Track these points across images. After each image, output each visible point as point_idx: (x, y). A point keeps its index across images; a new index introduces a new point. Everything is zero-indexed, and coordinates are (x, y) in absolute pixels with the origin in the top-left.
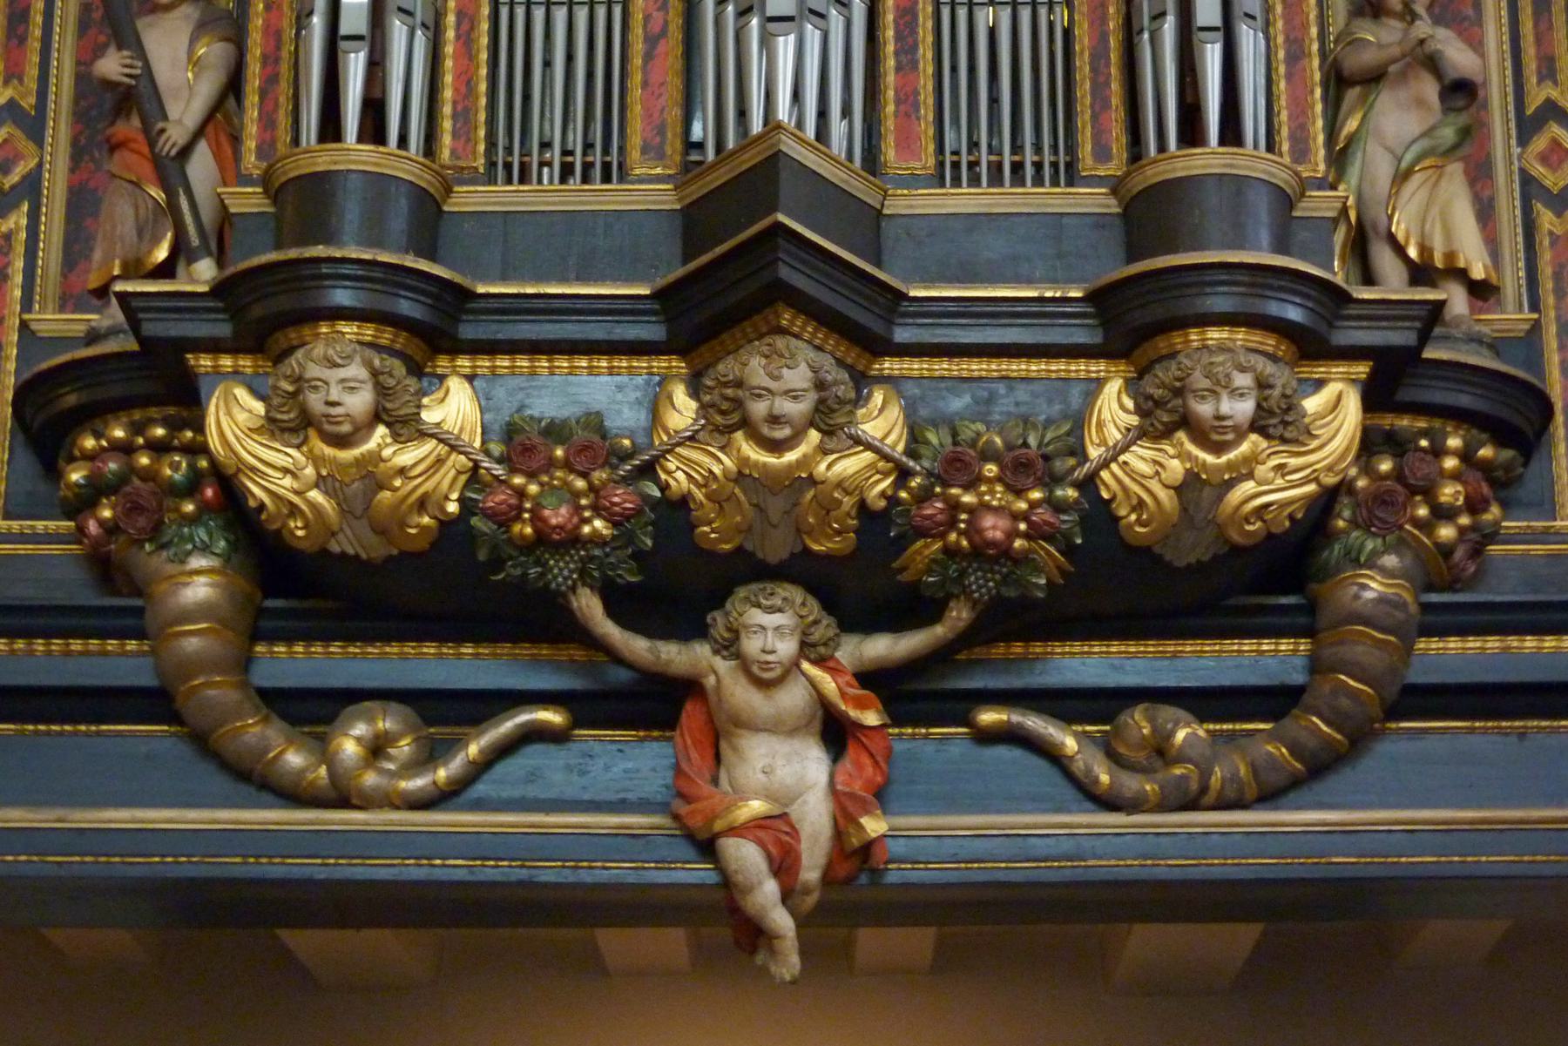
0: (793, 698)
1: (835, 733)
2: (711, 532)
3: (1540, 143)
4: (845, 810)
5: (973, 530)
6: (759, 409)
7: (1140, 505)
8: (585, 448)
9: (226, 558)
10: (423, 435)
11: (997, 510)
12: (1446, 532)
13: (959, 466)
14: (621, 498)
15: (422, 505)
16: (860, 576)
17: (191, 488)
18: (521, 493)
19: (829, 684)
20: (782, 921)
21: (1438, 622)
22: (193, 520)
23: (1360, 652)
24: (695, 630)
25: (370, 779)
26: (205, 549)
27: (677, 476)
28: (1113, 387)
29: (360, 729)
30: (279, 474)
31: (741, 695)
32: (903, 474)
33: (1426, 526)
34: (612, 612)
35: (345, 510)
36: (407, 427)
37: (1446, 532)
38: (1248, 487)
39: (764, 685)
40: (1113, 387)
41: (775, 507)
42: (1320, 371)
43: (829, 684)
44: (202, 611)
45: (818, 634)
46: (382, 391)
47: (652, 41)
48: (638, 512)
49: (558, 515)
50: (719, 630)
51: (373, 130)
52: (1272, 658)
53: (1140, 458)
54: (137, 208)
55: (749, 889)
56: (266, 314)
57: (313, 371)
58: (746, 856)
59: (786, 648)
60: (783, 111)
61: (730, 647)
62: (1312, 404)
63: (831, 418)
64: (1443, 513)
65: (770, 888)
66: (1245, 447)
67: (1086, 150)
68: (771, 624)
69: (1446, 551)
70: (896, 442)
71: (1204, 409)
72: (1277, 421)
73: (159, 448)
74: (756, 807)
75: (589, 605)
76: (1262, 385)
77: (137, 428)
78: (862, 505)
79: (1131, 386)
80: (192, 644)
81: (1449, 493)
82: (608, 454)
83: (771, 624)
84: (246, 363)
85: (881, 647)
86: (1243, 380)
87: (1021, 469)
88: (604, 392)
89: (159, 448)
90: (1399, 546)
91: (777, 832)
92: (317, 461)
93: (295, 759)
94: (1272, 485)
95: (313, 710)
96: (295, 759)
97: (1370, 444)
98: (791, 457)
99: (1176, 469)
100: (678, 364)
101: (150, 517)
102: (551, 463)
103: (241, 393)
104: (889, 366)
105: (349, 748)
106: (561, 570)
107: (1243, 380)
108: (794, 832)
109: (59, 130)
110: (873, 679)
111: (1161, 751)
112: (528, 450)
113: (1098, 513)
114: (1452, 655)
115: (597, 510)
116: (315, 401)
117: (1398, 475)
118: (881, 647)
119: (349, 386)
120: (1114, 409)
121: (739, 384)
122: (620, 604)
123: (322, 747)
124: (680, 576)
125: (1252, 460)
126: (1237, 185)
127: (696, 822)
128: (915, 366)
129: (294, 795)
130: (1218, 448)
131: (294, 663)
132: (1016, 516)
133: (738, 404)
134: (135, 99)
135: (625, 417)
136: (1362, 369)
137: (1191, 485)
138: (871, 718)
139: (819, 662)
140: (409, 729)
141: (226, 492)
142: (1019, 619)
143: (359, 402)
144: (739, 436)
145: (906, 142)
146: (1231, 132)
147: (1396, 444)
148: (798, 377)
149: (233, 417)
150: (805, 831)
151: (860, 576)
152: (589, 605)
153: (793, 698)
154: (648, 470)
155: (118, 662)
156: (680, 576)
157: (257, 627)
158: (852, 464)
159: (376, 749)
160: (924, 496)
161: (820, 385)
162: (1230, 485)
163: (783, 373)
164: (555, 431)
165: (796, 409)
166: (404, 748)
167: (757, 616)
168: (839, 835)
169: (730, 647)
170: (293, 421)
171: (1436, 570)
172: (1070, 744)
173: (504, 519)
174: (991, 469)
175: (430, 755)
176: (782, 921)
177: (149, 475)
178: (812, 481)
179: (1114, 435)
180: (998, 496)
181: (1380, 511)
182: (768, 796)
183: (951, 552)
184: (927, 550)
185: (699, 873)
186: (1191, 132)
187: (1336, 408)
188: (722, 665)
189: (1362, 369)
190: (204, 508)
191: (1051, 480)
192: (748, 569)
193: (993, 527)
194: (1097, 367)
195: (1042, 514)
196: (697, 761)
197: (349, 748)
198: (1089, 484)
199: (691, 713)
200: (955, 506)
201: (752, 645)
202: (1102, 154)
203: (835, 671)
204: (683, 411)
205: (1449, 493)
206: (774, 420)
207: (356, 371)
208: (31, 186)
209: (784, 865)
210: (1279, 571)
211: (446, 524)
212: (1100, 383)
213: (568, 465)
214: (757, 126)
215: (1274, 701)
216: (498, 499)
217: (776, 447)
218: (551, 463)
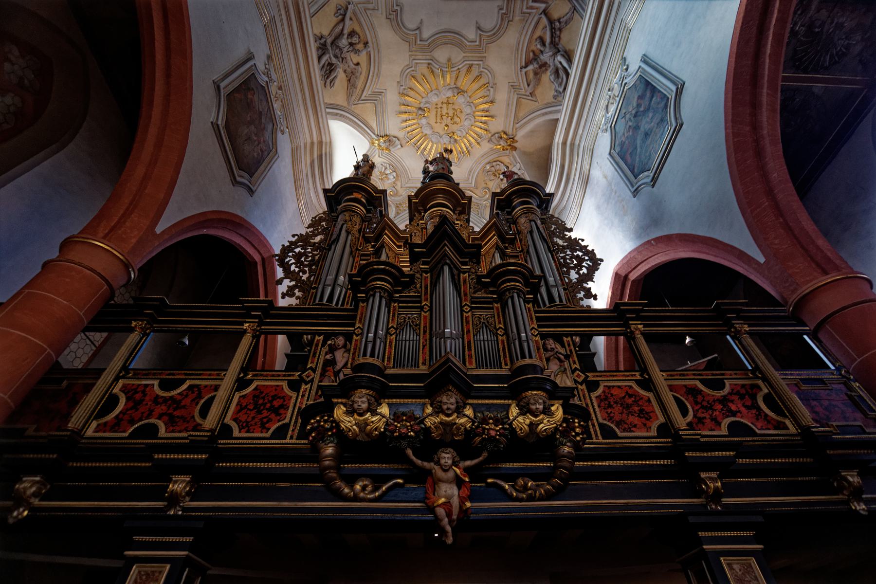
0: (450, 474)
3: (576, 374)
4: (462, 501)
5: (488, 434)
6: (445, 407)
7: (521, 429)
8: (410, 417)
9: (336, 444)
10: (377, 414)
11: (494, 430)
12: (578, 438)
13: (485, 421)
14: (417, 428)
15: (376, 429)
16: (465, 445)
17: (330, 429)
18: (396, 426)
19: (458, 471)
20: (449, 528)
22: (330, 436)
23: (565, 464)
24: (430, 460)
25: (362, 495)
26: (332, 442)
27: (428, 422)
28: (514, 405)
29: (361, 483)
30: (348, 422)
31: (440, 473)
32: (473, 422)
33: (575, 437)
34: (414, 455)
35: (360, 431)
36: (374, 413)
37: (578, 438)
38: (542, 425)
39: (445, 471)
40: (514, 405)
41: (448, 429)
42: (553, 402)
43: (458, 471)
44: (331, 455)
45: (456, 459)
46: (369, 404)
47: (424, 346)
48: (420, 431)
49: (404, 431)
50: (436, 459)
51: (372, 355)
53: (520, 419)
55: (441, 520)
56: (346, 389)
57: (356, 399)
58: (441, 512)
59: (450, 462)
60: (448, 350)
61: (438, 463)
62: (553, 408)
63: (459, 411)
64: (577, 434)
65: (446, 520)
66: (541, 417)
67: (503, 364)
68: (446, 457)
69: (579, 441)
70: (472, 416)
71: (533, 407)
72: (547, 411)
73: (325, 421)
74: (443, 500)
75: (409, 452)
76: (544, 402)
77: (322, 417)
78: (465, 428)
79: (517, 405)
80: (327, 463)
81: (578, 430)
84: (344, 401)
86: (541, 401)
87: (497, 422)
88: (413, 406)
89: (325, 421)
90: (570, 441)
91: (447, 505)
92: (355, 419)
93: (346, 490)
94: (545, 425)
95: (351, 480)
96: (346, 490)
97: (565, 420)
98: (451, 418)
99: (528, 422)
100: (427, 400)
101: (322, 434)
102: (403, 420)
103: (342, 407)
104: (470, 401)
105: (358, 487)
106: (404, 443)
107: (541, 401)
108: (451, 506)
110: (467, 470)
111: (525, 488)
112: (399, 417)
113: (513, 430)
115: (412, 431)
116: (356, 406)
117: (567, 426)
118: (468, 463)
119: (363, 402)
120: (514, 411)
121: (441, 402)
123: (352, 487)
125: (543, 419)
127: (430, 504)
128: (475, 401)
129: (345, 498)
130: (536, 416)
132: (497, 431)
133: (441, 406)
134: (332, 362)
135: (418, 413)
136: (561, 402)
137: (532, 425)
138: (467, 479)
139: (456, 466)
140: (371, 483)
142: (497, 456)
143: (365, 406)
144: (440, 415)
145: (471, 363)
146: (531, 357)
148: (453, 400)
149: (339, 412)
150: (454, 506)
152: (409, 452)
153: (450, 474)
154: (422, 422)
156: (429, 444)
158: (463, 420)
159: (364, 488)
160: (477, 427)
161: (457, 402)
162: (539, 425)
163: (450, 400)
164: (403, 414)
165: (453, 407)
166: (370, 488)
167: (444, 455)
168: (461, 507)
169: (438, 463)
170: (351, 411)
171: (576, 446)
172: (507, 487)
173: (393, 432)
174: (491, 421)
176: (449, 528)
177: (323, 426)
178: (455, 424)
179: (515, 414)
180: (493, 427)
181: (566, 433)
182: (445, 497)
183: (484, 439)
184: (478, 439)
185: (430, 517)
186: (523, 357)
187: (558, 411)
188: (436, 467)
189: (561, 402)
190: (333, 434)
191: (503, 424)
192: (442, 444)
193: (493, 433)
194: (510, 402)
195: (502, 431)
196: (430, 491)
197: (358, 487)
198: (511, 424)
199: (429, 480)
200: (485, 429)
201: (443, 461)
202: (506, 365)
203: (459, 468)
204: (429, 410)
205: (578, 430)
206: (448, 409)
207: (364, 399)
208: (312, 381)
209: (449, 514)
211: (381, 433)
212: (510, 405)
213: (406, 420)
214: (443, 354)
216: (392, 427)
217: (448, 416)
218: (403, 420)
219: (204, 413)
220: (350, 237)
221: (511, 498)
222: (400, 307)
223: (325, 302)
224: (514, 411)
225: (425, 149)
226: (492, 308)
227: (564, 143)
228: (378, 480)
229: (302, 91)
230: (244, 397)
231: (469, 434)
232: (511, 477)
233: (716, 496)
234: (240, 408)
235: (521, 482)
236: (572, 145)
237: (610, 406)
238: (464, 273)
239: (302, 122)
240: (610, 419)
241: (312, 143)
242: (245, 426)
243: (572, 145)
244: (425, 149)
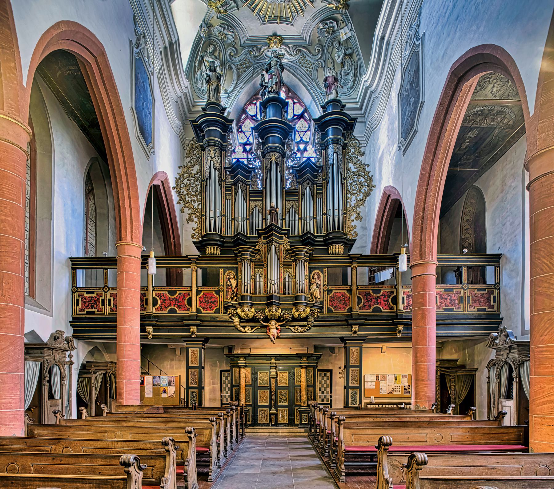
1: (277, 329)
2: (269, 317)
21: (315, 321)
24: (267, 322)
30: (242, 315)
31: (271, 327)
52: (305, 323)
54: (517, 161)
68: (273, 322)
82: (331, 371)
83: (273, 322)
85: (280, 324)
95: (244, 327)
97: (310, 310)
109: (279, 295)
110: (280, 326)
111: (297, 330)
113: (293, 316)
114: (316, 323)
118: (280, 324)
120: (294, 310)
122: (263, 322)
124: (267, 320)
126: (247, 296)
131: (242, 324)
141: (238, 315)
147: (313, 310)
149: (239, 311)
151: (279, 320)
155: (232, 324)
157: (240, 322)
175: (252, 329)
193: (287, 317)
210: (306, 319)
215: (305, 326)
219: (190, 304)
220: (217, 171)
221: (293, 332)
222: (256, 265)
223: (212, 232)
224: (294, 310)
225: (260, 10)
226: (291, 265)
227: (383, 38)
228: (252, 327)
229: (154, 11)
230: (200, 297)
231: (280, 317)
232: (294, 326)
233: (355, 332)
234: (201, 302)
235: (296, 327)
236: (388, 42)
237: (334, 301)
238: (281, 244)
239: (149, 15)
240: (332, 306)
241: (165, 48)
242: (204, 308)
243: (388, 42)
244: (260, 10)
